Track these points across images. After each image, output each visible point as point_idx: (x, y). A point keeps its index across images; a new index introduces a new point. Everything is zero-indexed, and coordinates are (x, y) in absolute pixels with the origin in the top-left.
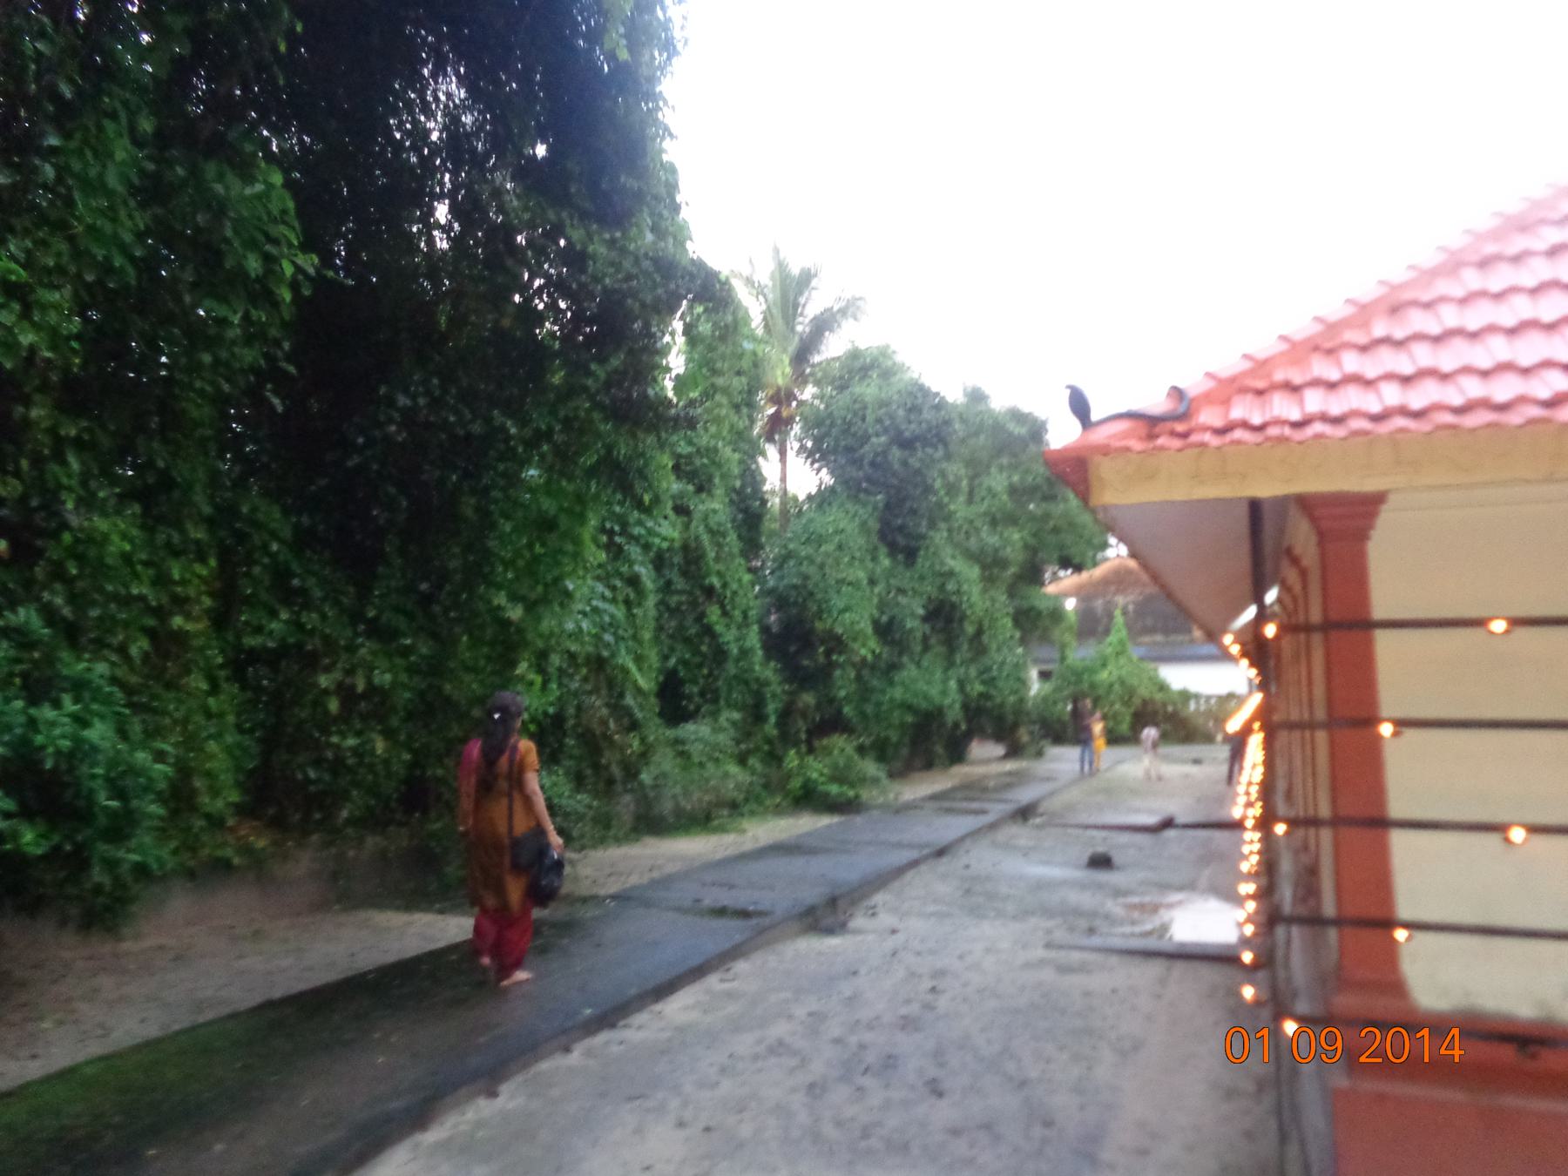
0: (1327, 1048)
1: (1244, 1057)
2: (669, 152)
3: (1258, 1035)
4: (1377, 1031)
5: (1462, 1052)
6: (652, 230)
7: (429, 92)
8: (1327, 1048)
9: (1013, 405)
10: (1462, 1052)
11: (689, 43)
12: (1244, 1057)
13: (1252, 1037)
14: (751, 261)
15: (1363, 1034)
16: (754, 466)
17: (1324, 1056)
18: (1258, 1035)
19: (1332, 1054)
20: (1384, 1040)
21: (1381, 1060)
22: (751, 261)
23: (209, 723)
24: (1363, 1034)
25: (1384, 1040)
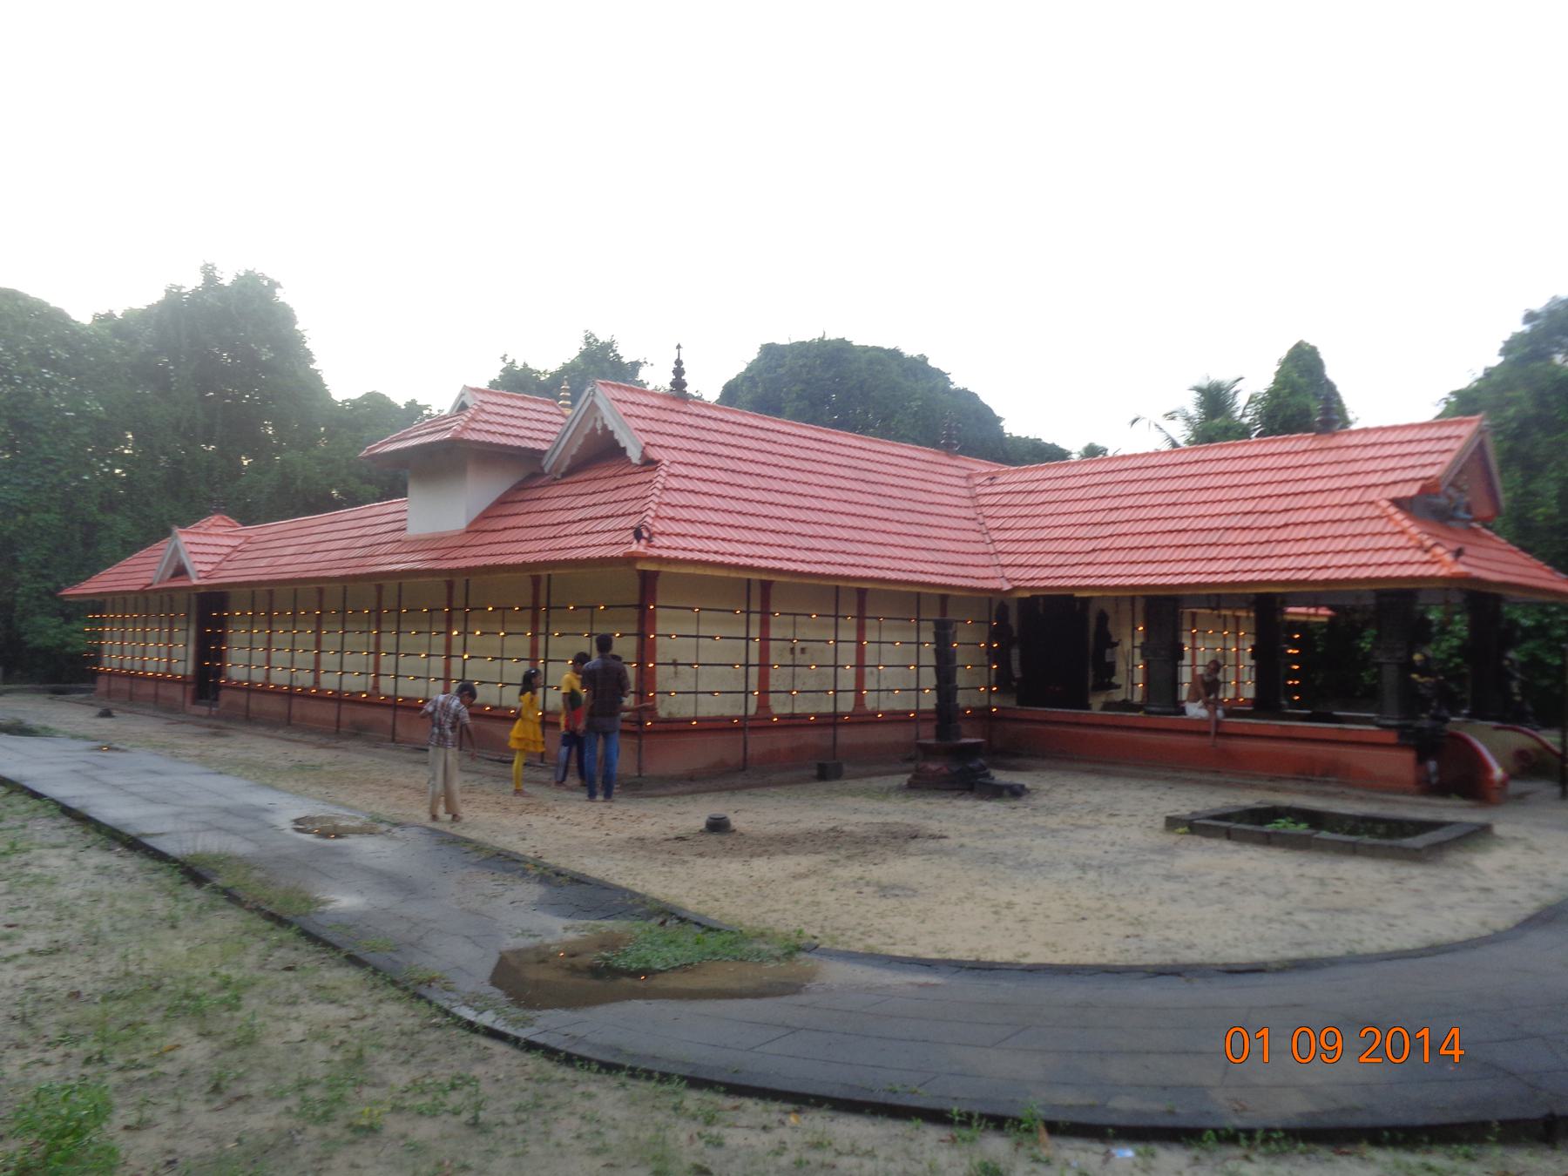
0: (1328, 1048)
1: (1244, 1058)
2: (282, 284)
3: (1258, 1035)
4: (1377, 1032)
5: (1463, 1052)
6: (281, 940)
7: (1549, 660)
8: (1328, 1048)
9: (298, 319)
10: (1463, 1052)
11: (1133, 418)
12: (1244, 1058)
13: (1252, 1037)
14: (1241, 379)
15: (1363, 1034)
16: (867, 1111)
17: (1323, 1056)
18: (1258, 1035)
19: (1332, 1054)
20: (1384, 1039)
21: (1380, 1060)
22: (1241, 379)
23: (1018, 707)
24: (1363, 1034)
25: (1384, 1039)
